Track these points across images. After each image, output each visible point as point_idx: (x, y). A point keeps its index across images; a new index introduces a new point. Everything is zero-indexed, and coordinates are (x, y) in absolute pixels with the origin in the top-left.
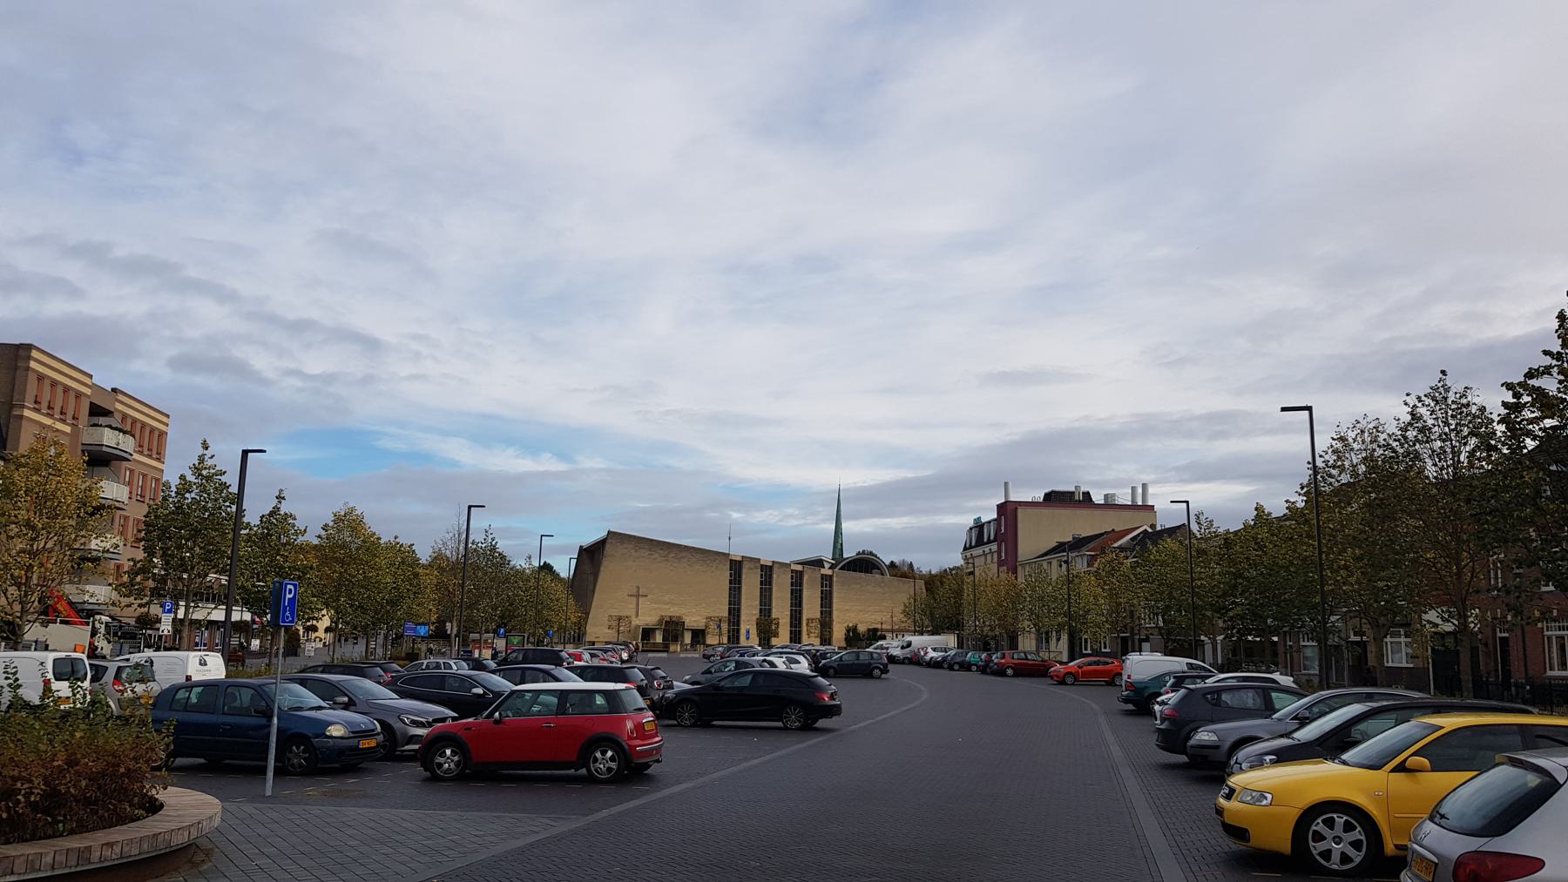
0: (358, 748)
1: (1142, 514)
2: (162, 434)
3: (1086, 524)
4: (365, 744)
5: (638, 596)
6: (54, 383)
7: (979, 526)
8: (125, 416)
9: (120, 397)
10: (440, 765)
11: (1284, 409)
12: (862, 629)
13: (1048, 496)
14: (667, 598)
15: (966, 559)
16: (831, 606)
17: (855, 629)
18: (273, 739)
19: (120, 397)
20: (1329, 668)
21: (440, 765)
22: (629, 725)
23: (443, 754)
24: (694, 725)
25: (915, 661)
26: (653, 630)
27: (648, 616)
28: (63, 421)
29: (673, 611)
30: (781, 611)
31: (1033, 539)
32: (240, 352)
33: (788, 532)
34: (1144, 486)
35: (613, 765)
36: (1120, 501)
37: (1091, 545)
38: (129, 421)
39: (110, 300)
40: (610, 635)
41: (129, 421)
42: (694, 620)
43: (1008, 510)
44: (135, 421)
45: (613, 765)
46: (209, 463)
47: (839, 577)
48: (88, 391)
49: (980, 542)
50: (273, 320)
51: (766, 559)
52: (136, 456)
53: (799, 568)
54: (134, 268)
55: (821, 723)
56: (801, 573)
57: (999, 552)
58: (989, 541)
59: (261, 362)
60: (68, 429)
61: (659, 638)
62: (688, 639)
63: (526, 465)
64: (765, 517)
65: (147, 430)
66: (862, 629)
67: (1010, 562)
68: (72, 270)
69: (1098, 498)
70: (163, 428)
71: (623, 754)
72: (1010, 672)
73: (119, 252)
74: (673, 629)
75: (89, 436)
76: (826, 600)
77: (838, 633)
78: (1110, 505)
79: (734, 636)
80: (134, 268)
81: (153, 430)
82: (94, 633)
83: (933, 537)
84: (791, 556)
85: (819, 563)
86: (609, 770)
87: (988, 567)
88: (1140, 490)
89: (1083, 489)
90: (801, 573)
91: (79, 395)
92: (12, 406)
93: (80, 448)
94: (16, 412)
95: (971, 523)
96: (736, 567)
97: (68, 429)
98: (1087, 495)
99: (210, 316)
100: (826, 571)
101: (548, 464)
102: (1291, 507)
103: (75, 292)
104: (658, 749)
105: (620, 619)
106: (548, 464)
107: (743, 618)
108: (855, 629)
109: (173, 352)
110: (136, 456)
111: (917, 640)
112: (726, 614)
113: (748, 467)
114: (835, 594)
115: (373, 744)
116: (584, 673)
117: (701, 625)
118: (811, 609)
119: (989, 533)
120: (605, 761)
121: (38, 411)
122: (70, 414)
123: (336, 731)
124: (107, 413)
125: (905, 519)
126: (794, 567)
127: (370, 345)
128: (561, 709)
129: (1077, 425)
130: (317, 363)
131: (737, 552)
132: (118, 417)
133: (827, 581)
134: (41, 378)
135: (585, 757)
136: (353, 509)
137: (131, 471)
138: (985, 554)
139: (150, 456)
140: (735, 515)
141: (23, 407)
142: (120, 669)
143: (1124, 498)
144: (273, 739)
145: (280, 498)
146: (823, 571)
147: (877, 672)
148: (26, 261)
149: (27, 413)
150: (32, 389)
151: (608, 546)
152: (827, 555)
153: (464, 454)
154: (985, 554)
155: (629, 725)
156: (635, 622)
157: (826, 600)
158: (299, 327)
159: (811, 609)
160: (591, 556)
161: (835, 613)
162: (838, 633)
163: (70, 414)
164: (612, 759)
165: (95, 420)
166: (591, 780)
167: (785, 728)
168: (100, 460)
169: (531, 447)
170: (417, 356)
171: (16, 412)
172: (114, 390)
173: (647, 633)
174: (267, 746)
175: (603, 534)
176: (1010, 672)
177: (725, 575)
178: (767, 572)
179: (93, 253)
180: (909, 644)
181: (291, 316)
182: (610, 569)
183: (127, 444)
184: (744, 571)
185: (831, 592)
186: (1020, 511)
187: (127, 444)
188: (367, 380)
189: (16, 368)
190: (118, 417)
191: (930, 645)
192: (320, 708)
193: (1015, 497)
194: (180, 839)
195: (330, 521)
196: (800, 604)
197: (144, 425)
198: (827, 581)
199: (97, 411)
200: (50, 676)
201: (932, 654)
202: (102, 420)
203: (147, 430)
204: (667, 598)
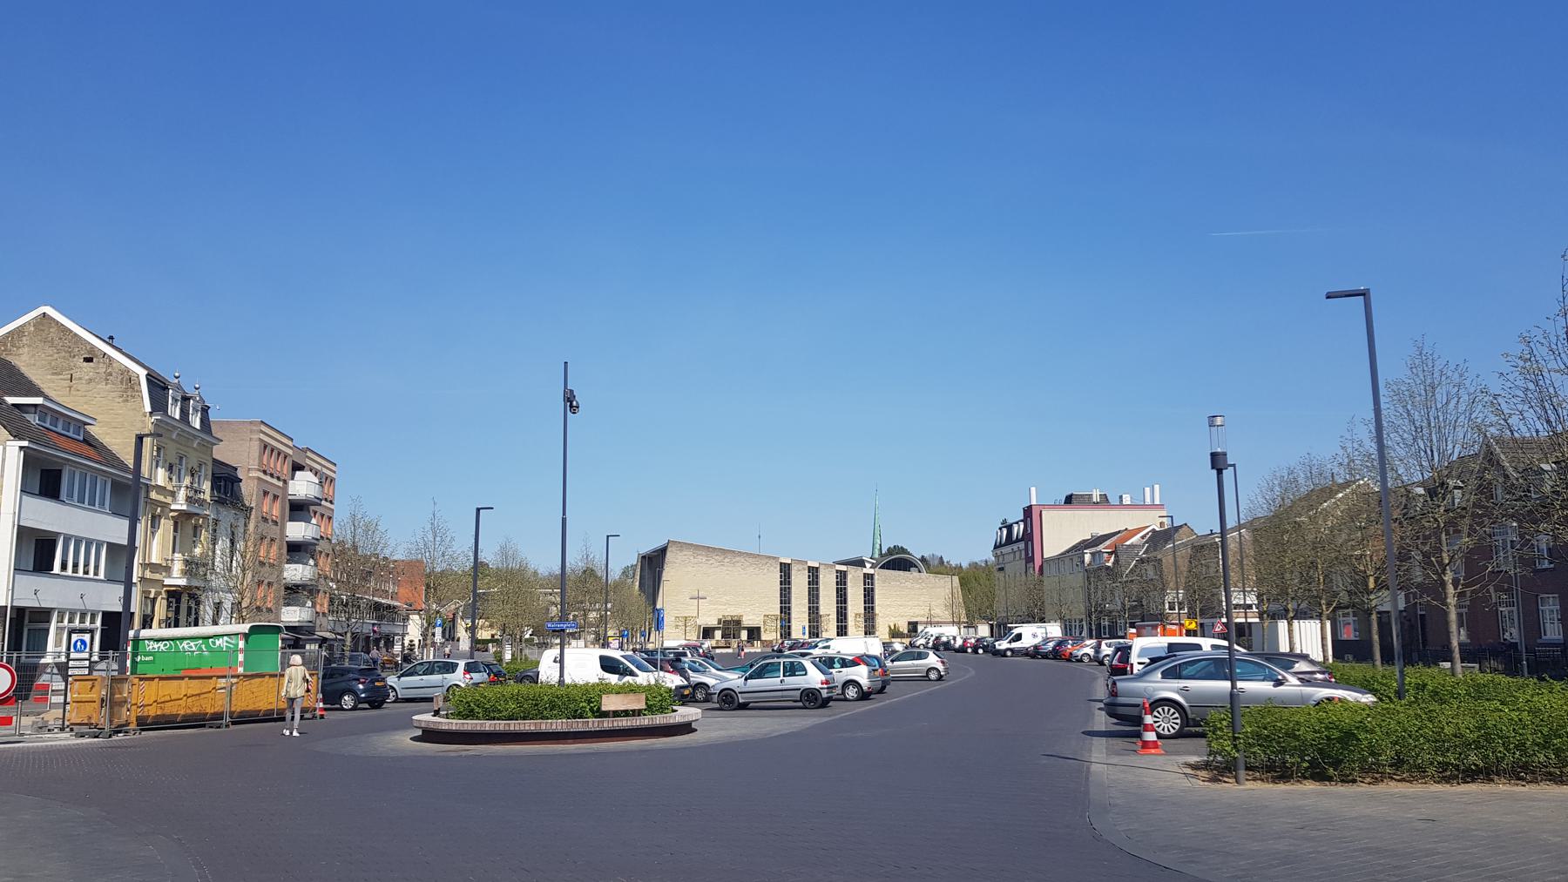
15: (996, 556)
20: (177, 611)
26: (714, 629)
29: (730, 612)
30: (828, 606)
37: (1108, 543)
47: (881, 576)
48: (290, 452)
53: (843, 568)
58: (1018, 540)
62: (744, 635)
74: (731, 627)
79: (786, 632)
85: (860, 563)
100: (868, 570)
107: (793, 615)
112: (862, 611)
114: (877, 591)
116: (1198, 647)
123: (1463, 638)
126: (839, 567)
133: (869, 578)
146: (865, 571)
151: (669, 555)
159: (855, 605)
177: (776, 576)
184: (793, 573)
198: (869, 578)
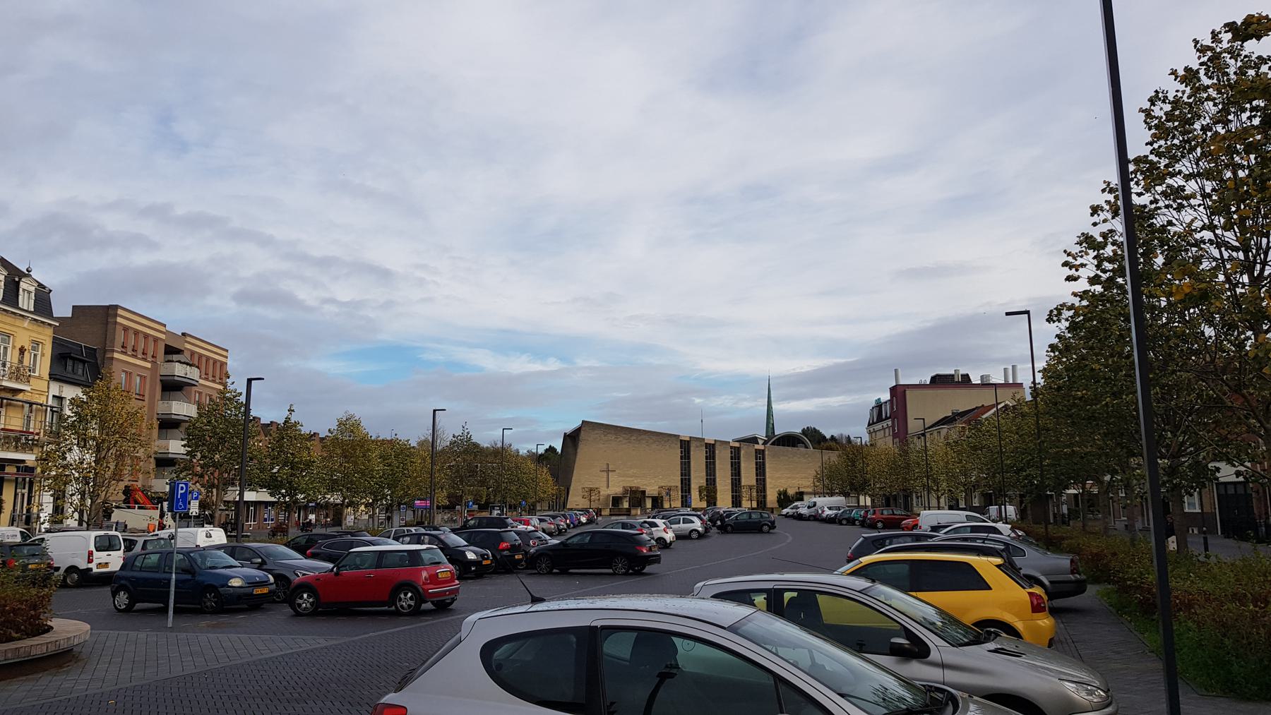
0: (252, 594)
1: (1013, 390)
2: (223, 364)
3: (962, 401)
4: (258, 591)
5: (608, 471)
6: (137, 332)
7: (879, 405)
8: (193, 353)
9: (188, 339)
10: (300, 605)
11: (1007, 314)
12: (791, 492)
13: (934, 379)
14: (630, 472)
16: (764, 474)
17: (785, 492)
18: (173, 589)
19: (188, 339)
21: (300, 605)
22: (424, 574)
23: (302, 597)
24: (626, 574)
25: (816, 518)
27: (616, 489)
28: (145, 360)
31: (921, 412)
32: (287, 286)
33: (734, 416)
34: (1014, 367)
35: (412, 603)
36: (993, 381)
37: (965, 418)
38: (196, 357)
39: (179, 251)
40: (584, 504)
41: (196, 357)
42: (652, 490)
43: (898, 392)
44: (201, 356)
45: (412, 603)
46: (232, 387)
48: (163, 337)
49: (880, 419)
50: (304, 258)
51: (710, 438)
52: (201, 381)
53: (737, 445)
54: (194, 223)
55: (648, 569)
56: (739, 449)
57: (893, 426)
58: (887, 418)
59: (305, 294)
60: (149, 365)
61: (626, 505)
62: (649, 504)
63: (537, 367)
64: (722, 402)
65: (204, 360)
66: (791, 492)
67: (901, 434)
68: (146, 227)
69: (975, 380)
70: (223, 359)
71: (420, 597)
72: (880, 525)
73: (180, 211)
75: (165, 369)
76: (761, 470)
77: (772, 497)
78: (985, 384)
80: (194, 223)
81: (215, 361)
82: (162, 515)
83: (846, 412)
84: (730, 437)
85: (754, 440)
86: (410, 606)
87: (887, 443)
88: (1010, 372)
89: (963, 371)
90: (739, 449)
91: (156, 340)
92: (105, 351)
93: (159, 378)
94: (108, 355)
95: (874, 404)
96: (685, 446)
97: (149, 365)
98: (966, 378)
99: (257, 262)
101: (553, 365)
102: (551, 449)
103: (152, 245)
104: (457, 590)
105: (591, 490)
106: (553, 365)
108: (785, 492)
109: (234, 289)
110: (201, 381)
111: (820, 501)
113: (714, 362)
114: (767, 465)
115: (265, 590)
117: (655, 494)
118: (748, 477)
119: (887, 410)
120: (406, 600)
121: (125, 353)
122: (150, 353)
123: (236, 583)
124: (179, 352)
125: (840, 398)
127: (384, 275)
128: (379, 565)
129: (981, 310)
130: (345, 292)
131: (685, 434)
132: (187, 354)
133: (760, 454)
134: (126, 329)
135: (393, 597)
136: (352, 416)
137: (200, 393)
138: (883, 429)
139: (214, 381)
140: (698, 401)
141: (113, 351)
142: (145, 542)
143: (998, 378)
144: (173, 589)
145: (291, 411)
146: (757, 447)
147: (766, 528)
148: (113, 223)
149: (116, 355)
150: (120, 337)
152: (761, 434)
153: (488, 362)
154: (883, 429)
155: (424, 574)
156: (605, 492)
157: (761, 470)
158: (325, 263)
159: (748, 477)
160: (572, 439)
161: (768, 480)
162: (772, 497)
163: (150, 353)
164: (411, 598)
165: (170, 357)
166: (397, 613)
167: (614, 574)
168: (172, 387)
169: (539, 353)
170: (421, 282)
171: (108, 355)
172: (184, 334)
173: (617, 500)
174: (168, 593)
175: (577, 424)
176: (880, 525)
177: (677, 452)
178: (711, 449)
179: (159, 213)
180: (815, 505)
181: (316, 253)
182: (585, 451)
183: (193, 373)
185: (764, 464)
186: (907, 392)
187: (193, 373)
188: (388, 305)
189: (107, 323)
190: (187, 354)
191: (827, 504)
192: (231, 567)
193: (902, 382)
194: (64, 645)
195: (334, 426)
196: (739, 474)
197: (208, 358)
198: (760, 454)
199: (170, 350)
200: (92, 548)
201: (828, 512)
202: (175, 357)
203: (204, 360)
204: (630, 472)
